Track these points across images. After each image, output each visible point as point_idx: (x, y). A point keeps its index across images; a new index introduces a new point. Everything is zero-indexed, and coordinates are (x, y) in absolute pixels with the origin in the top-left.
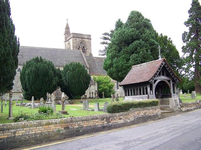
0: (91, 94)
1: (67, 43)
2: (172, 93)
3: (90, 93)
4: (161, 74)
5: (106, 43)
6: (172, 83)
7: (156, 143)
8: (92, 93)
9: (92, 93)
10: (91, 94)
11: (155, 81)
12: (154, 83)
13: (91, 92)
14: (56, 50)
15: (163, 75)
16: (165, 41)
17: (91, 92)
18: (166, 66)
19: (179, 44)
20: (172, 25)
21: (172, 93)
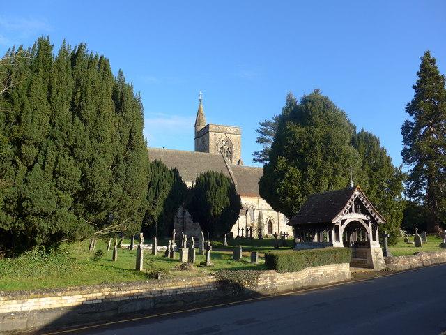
0: (241, 231)
1: (200, 140)
2: (371, 239)
3: (239, 229)
4: (353, 210)
5: (267, 141)
6: (370, 225)
7: (20, 325)
8: (243, 229)
9: (243, 229)
10: (241, 231)
11: (343, 221)
12: (342, 224)
13: (241, 229)
14: (179, 154)
15: (356, 211)
16: (367, 144)
17: (241, 229)
18: (361, 199)
19: (393, 147)
20: (380, 114)
21: (371, 239)
